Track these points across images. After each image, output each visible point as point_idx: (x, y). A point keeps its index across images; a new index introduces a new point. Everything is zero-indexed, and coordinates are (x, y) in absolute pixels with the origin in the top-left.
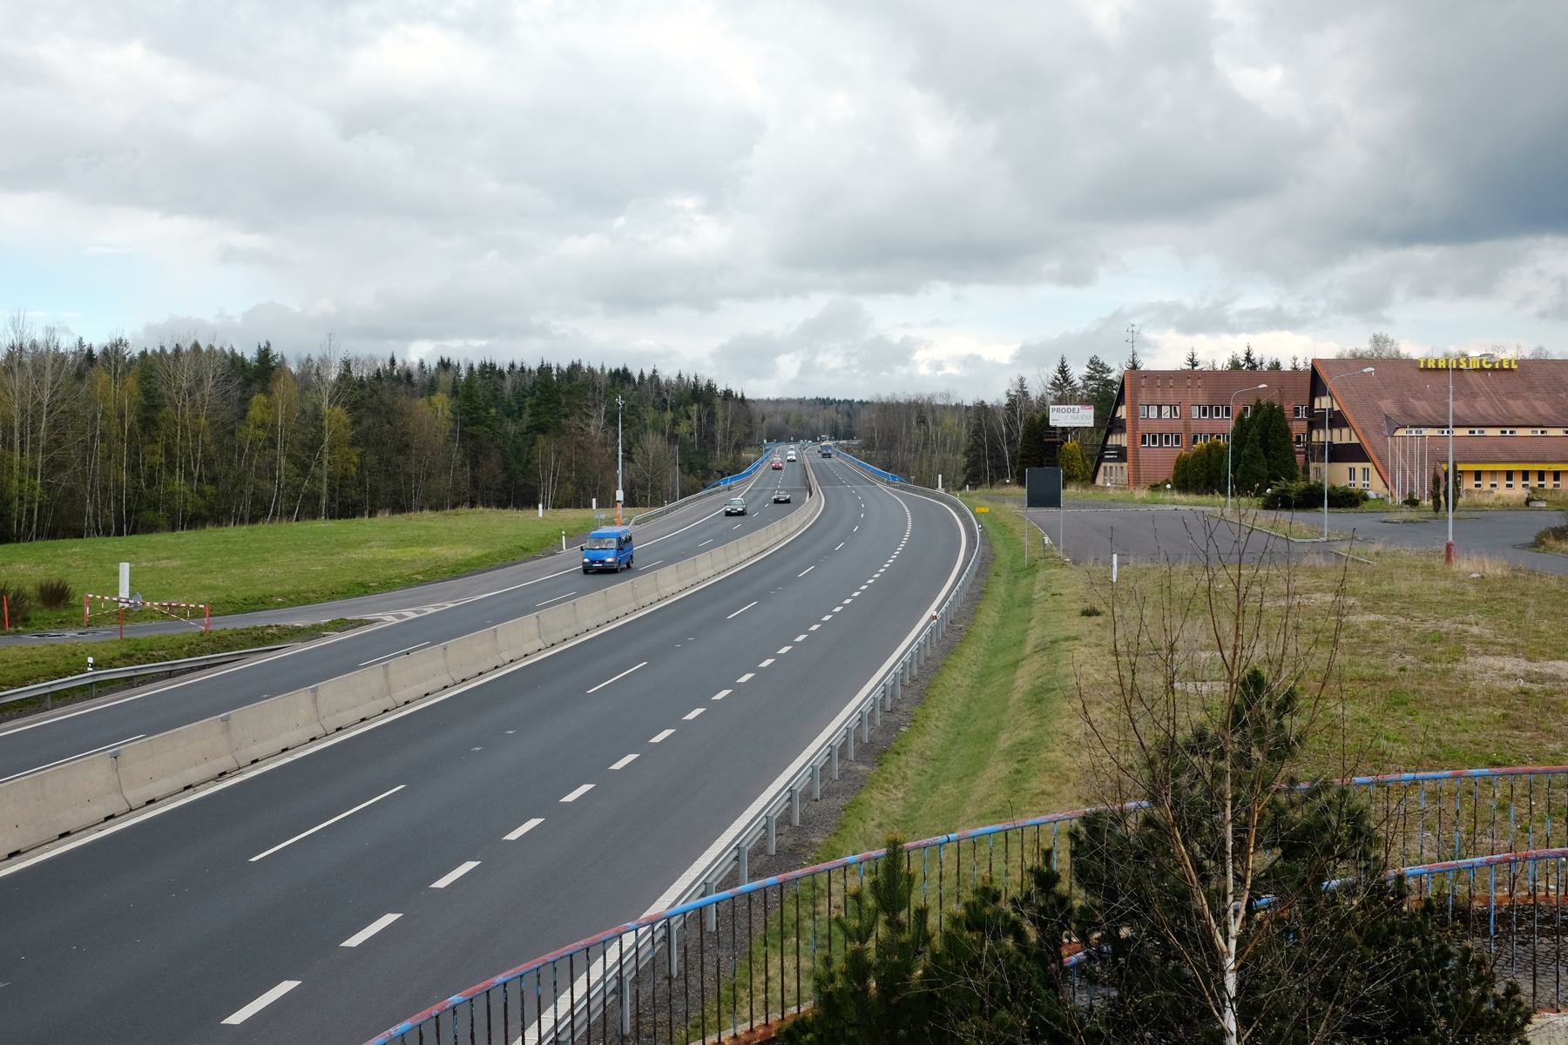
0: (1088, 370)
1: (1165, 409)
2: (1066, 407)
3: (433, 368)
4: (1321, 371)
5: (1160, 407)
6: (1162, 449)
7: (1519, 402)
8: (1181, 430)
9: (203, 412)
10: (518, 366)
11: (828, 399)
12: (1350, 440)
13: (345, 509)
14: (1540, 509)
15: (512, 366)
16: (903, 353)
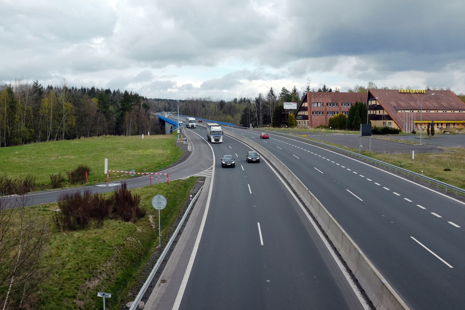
0: (282, 91)
1: (319, 105)
2: (289, 103)
3: (46, 89)
4: (372, 92)
5: (317, 103)
6: (318, 116)
7: (428, 103)
8: (324, 110)
9: (257, 109)
10: (75, 88)
11: (159, 99)
12: (380, 113)
13: (70, 136)
14: (447, 134)
15: (73, 88)
16: (170, 85)
